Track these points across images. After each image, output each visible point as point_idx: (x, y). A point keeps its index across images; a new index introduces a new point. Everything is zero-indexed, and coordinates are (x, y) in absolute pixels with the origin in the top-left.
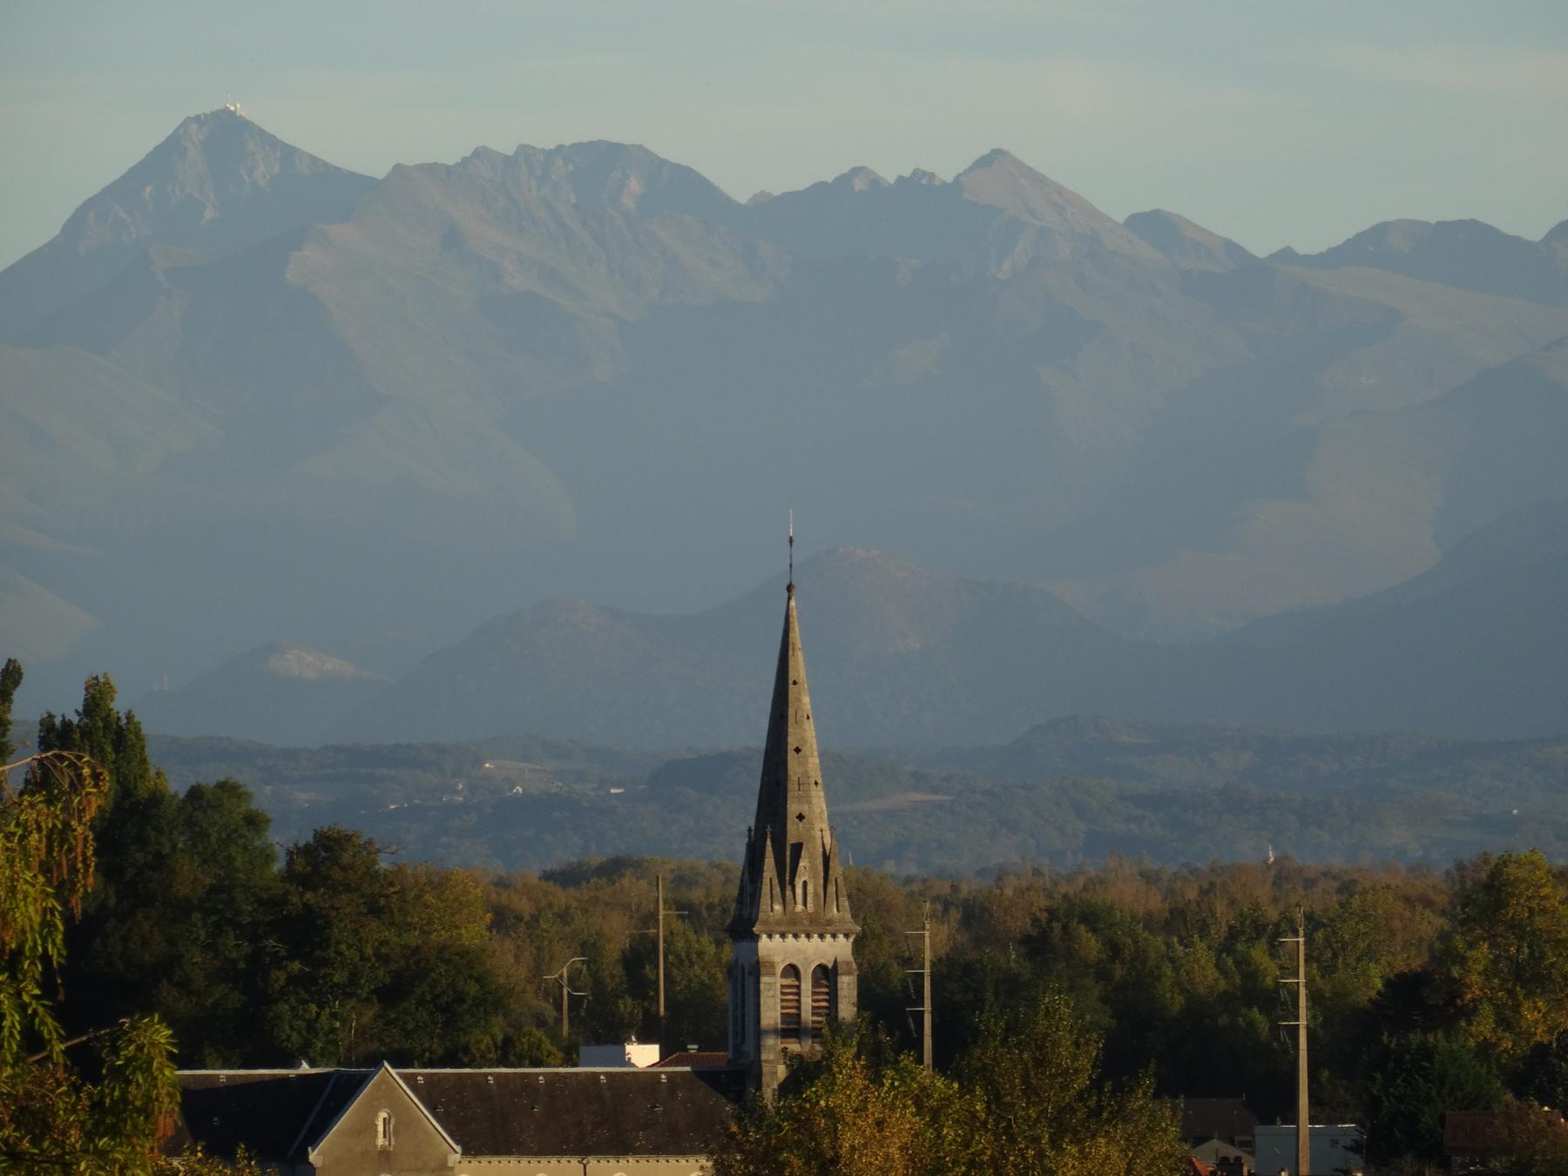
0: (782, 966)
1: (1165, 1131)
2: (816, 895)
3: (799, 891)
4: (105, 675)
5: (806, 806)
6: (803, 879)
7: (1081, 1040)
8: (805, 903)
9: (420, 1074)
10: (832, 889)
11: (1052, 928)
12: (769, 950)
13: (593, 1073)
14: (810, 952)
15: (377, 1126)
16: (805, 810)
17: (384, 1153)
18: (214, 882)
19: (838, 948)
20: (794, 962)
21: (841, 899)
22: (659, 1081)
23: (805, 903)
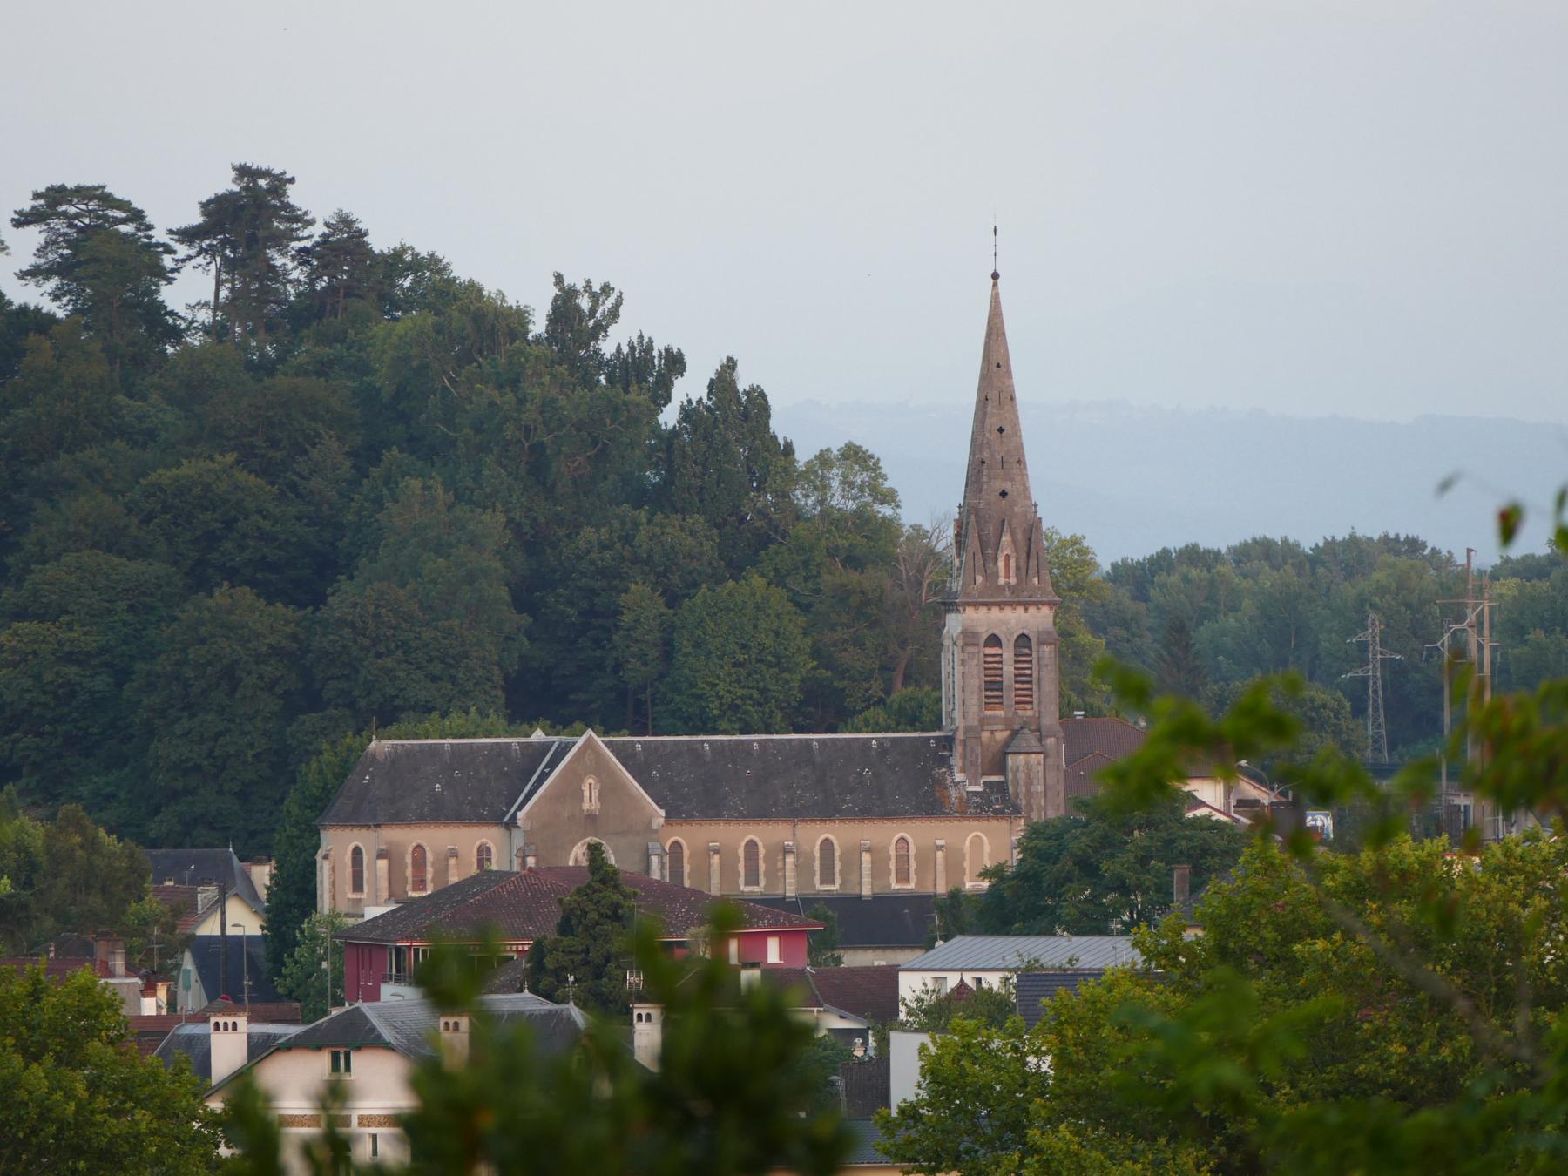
0: (985, 636)
1: (160, 475)
2: (1018, 568)
3: (1001, 564)
4: (16, 212)
5: (1010, 484)
6: (1005, 553)
7: (188, 1074)
8: (1007, 576)
9: (873, 739)
10: (1033, 562)
11: (963, 1066)
12: (972, 620)
13: (806, 740)
14: (1013, 622)
15: (582, 791)
16: (1008, 486)
17: (591, 818)
18: (1444, 817)
19: (1038, 619)
20: (997, 632)
21: (1042, 572)
22: (870, 747)
23: (1007, 576)
